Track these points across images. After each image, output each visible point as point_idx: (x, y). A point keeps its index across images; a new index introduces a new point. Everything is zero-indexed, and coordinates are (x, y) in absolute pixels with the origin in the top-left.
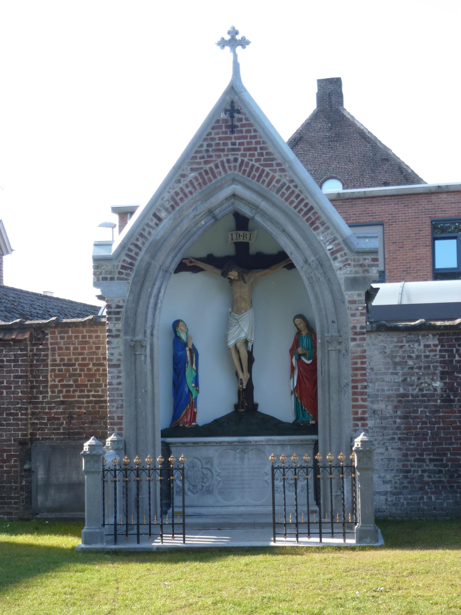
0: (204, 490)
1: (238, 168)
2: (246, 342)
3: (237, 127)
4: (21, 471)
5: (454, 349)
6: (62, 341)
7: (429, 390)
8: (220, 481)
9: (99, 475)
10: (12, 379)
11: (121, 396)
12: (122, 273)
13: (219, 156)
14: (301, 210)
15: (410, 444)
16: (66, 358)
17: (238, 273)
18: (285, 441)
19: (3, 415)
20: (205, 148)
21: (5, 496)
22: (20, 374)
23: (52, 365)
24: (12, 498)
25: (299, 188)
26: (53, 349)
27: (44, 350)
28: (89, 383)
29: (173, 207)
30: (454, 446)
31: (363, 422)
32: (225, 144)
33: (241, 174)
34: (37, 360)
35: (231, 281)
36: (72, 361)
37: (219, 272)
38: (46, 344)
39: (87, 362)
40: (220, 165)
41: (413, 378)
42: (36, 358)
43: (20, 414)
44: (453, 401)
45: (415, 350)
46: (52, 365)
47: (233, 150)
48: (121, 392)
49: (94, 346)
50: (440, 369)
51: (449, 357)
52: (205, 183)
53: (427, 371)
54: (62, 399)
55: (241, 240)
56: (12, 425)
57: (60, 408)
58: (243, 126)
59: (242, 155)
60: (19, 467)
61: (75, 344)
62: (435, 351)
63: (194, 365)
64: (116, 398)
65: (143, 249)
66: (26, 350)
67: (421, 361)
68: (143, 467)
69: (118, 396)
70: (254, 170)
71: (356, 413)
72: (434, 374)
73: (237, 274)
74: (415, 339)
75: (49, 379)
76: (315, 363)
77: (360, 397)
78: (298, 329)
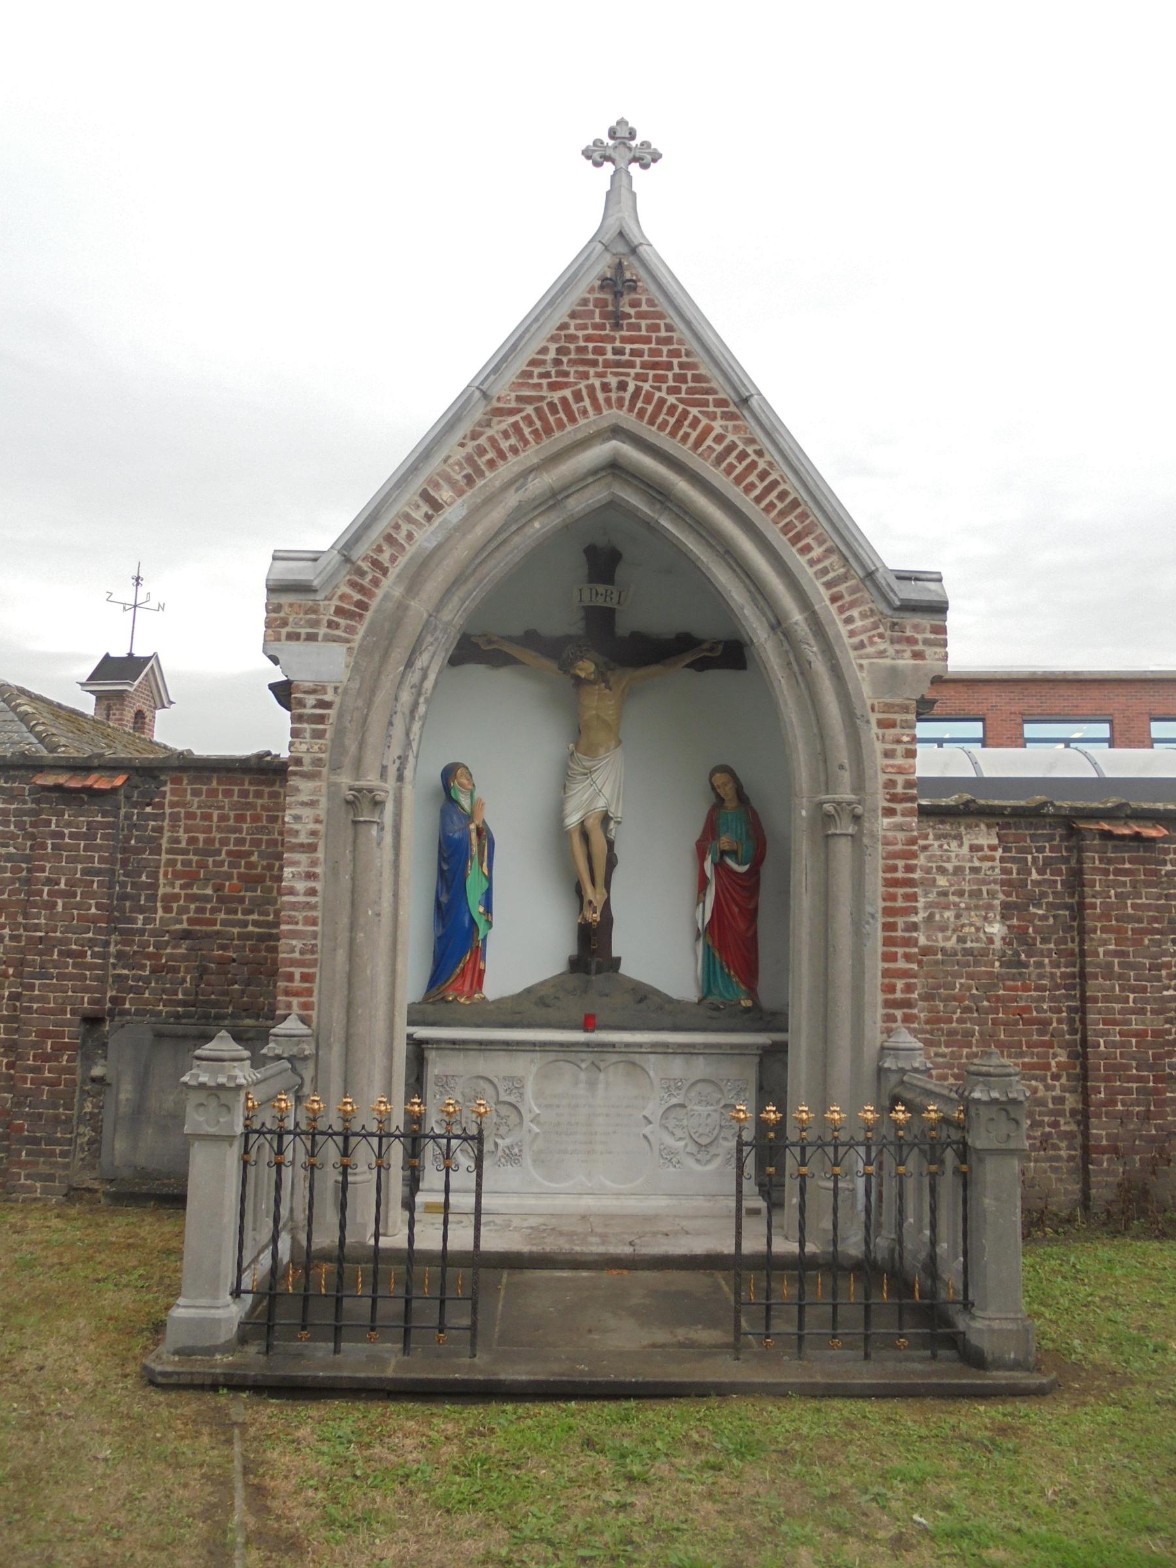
0: (500, 1153)
1: (627, 403)
2: (606, 819)
3: (629, 316)
4: (84, 1082)
5: (1029, 857)
6: (196, 799)
7: (978, 940)
8: (537, 1134)
9: (231, 1145)
10: (78, 876)
11: (314, 923)
12: (337, 626)
13: (585, 376)
14: (772, 506)
15: (937, 1055)
16: (201, 837)
17: (596, 665)
18: (693, 1046)
19: (52, 955)
20: (552, 354)
21: (41, 1138)
22: (96, 865)
23: (170, 851)
24: (58, 1142)
25: (768, 457)
26: (175, 817)
27: (155, 817)
28: (248, 894)
29: (469, 480)
30: (1026, 1060)
31: (906, 1010)
32: (600, 351)
33: (633, 416)
34: (139, 839)
35: (579, 682)
36: (213, 845)
37: (552, 665)
38: (161, 806)
39: (247, 848)
40: (584, 393)
41: (947, 914)
42: (135, 833)
43: (89, 953)
44: (1026, 966)
45: (953, 855)
46: (170, 851)
47: (618, 364)
48: (315, 914)
49: (264, 814)
50: (1001, 896)
51: (1018, 874)
52: (548, 431)
53: (974, 902)
54: (185, 926)
55: (600, 602)
56: (71, 977)
57: (180, 947)
58: (641, 315)
59: (638, 377)
60: (79, 1071)
61: (222, 808)
62: (993, 859)
63: (485, 864)
64: (300, 927)
65: (391, 570)
66: (116, 816)
67: (964, 879)
68: (363, 1127)
69: (305, 924)
70: (665, 410)
71: (891, 989)
72: (990, 907)
73: (592, 668)
74: (953, 833)
75: (162, 881)
76: (754, 872)
77: (900, 951)
78: (718, 796)
